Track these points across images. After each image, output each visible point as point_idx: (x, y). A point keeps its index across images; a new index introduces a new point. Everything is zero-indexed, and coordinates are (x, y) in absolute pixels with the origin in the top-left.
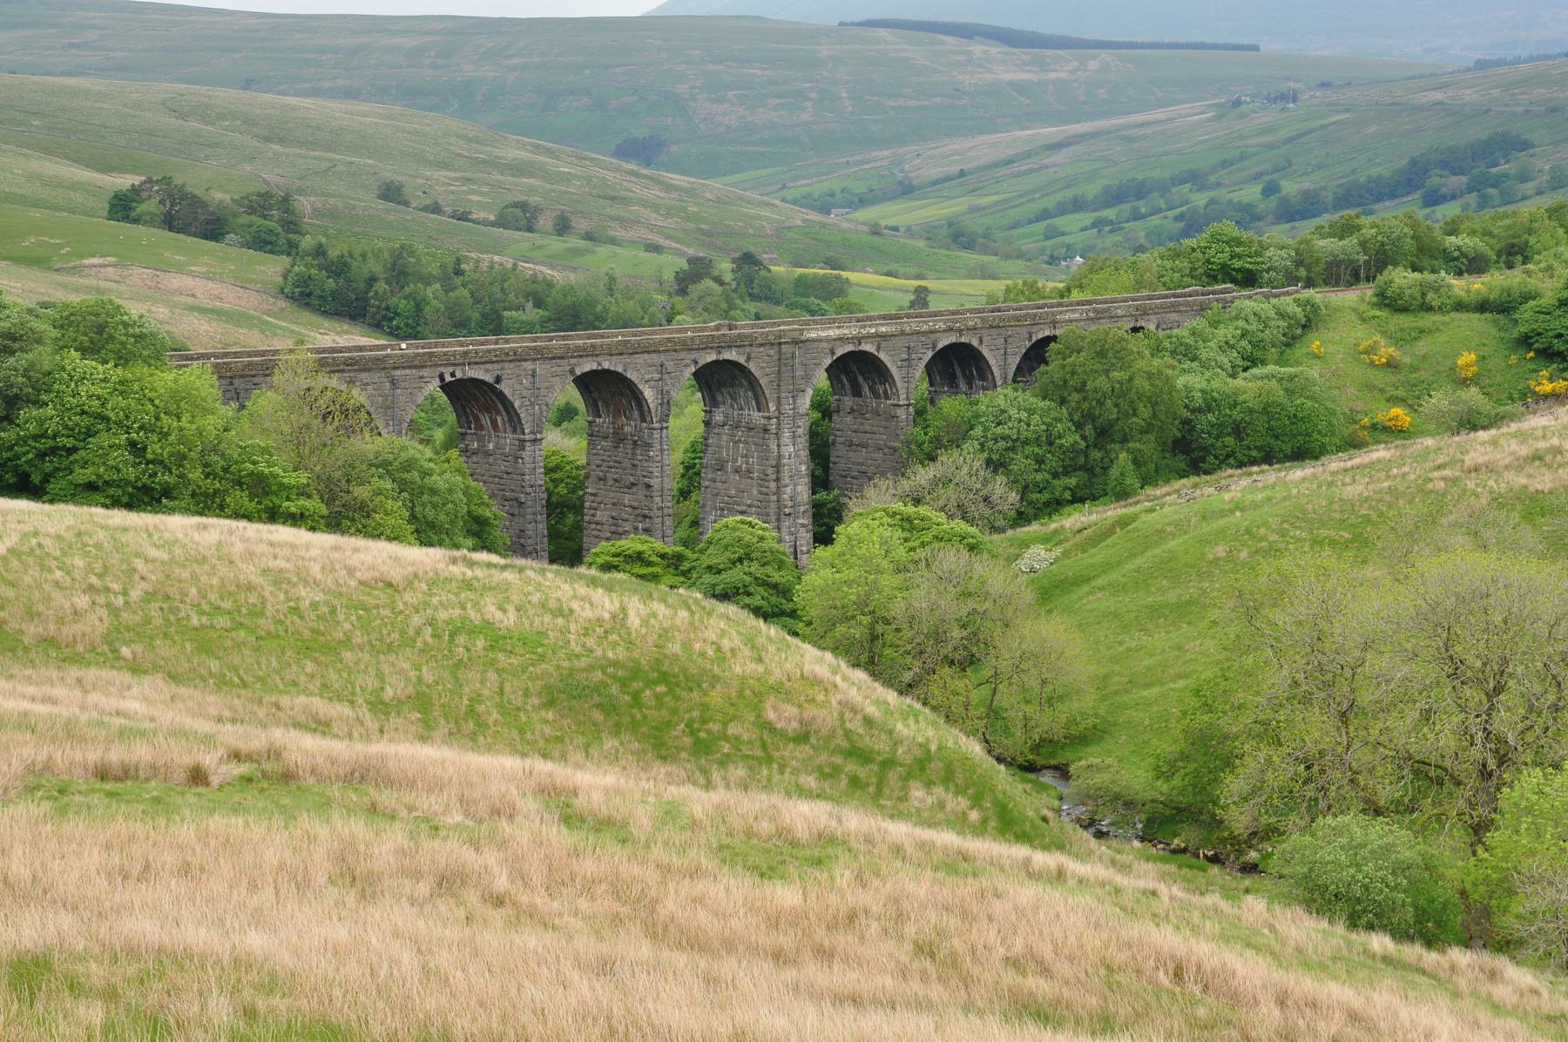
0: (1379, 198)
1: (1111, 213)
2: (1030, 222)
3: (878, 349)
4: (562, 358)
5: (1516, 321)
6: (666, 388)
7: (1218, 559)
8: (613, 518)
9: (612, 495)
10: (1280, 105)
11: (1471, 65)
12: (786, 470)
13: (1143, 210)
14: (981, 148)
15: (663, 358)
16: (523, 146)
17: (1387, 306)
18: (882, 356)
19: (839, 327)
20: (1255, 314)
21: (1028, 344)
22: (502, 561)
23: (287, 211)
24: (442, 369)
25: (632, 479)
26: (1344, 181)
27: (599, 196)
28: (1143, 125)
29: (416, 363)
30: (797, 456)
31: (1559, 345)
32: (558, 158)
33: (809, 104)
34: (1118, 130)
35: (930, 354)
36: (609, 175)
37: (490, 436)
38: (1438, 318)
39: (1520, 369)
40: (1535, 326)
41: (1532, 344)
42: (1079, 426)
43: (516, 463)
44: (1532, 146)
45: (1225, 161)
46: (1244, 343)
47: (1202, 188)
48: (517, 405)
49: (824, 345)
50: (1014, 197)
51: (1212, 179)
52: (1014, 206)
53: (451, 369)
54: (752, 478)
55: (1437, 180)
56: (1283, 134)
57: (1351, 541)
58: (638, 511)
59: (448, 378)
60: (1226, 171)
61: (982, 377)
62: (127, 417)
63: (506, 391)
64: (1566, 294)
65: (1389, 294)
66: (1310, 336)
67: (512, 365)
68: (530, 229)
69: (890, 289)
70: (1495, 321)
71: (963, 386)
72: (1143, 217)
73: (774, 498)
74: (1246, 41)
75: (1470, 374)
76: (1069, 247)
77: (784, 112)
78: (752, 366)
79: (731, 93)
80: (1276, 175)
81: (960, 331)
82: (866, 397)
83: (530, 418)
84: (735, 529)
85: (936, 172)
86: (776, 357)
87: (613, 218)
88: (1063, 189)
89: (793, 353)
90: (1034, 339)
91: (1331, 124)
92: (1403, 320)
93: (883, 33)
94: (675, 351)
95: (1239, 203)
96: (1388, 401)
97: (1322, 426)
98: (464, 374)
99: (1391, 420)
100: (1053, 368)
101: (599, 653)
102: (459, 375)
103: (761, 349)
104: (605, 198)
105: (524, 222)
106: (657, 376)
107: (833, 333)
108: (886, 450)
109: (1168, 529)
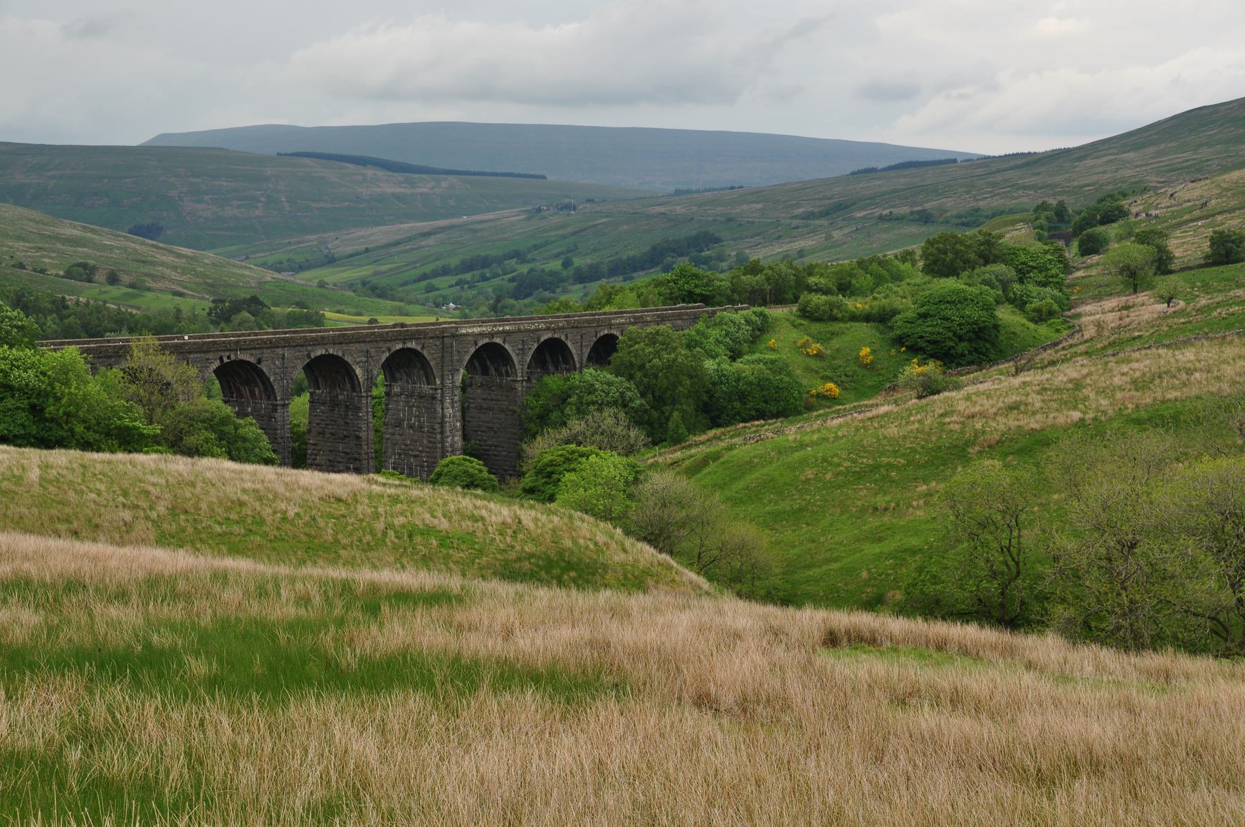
0: (635, 270)
1: (468, 276)
2: (414, 282)
3: (504, 342)
4: (302, 346)
6: (370, 368)
8: (330, 461)
9: (329, 444)
10: (566, 212)
13: (488, 275)
14: (379, 234)
17: (807, 317)
18: (507, 346)
19: (480, 326)
22: (397, 482)
24: (222, 354)
26: (612, 259)
27: (133, 260)
28: (482, 222)
34: (466, 225)
35: (536, 345)
36: (138, 247)
37: (248, 402)
38: (842, 325)
39: (898, 359)
41: (904, 343)
42: (643, 395)
43: (270, 421)
44: (722, 241)
45: (535, 246)
46: (728, 340)
47: (524, 261)
48: (272, 379)
49: (470, 338)
50: (403, 266)
51: (530, 256)
53: (227, 354)
54: (423, 432)
55: (670, 259)
56: (570, 230)
58: (351, 456)
59: (226, 360)
60: (537, 251)
63: (265, 369)
65: (808, 309)
66: (766, 336)
67: (269, 351)
68: (90, 281)
69: (346, 321)
71: (551, 368)
72: (488, 279)
73: (440, 445)
74: (538, 173)
76: (444, 297)
77: (244, 210)
78: (425, 353)
79: (206, 197)
80: (569, 255)
81: (554, 330)
82: (492, 375)
83: (281, 389)
84: (459, 465)
85: (349, 249)
86: (441, 347)
87: (146, 275)
88: (434, 261)
89: (452, 344)
90: (598, 336)
91: (600, 224)
92: (817, 327)
93: (306, 160)
94: (376, 341)
99: (827, 391)
101: (518, 548)
102: (233, 357)
103: (431, 341)
106: (364, 359)
107: (476, 330)
108: (508, 412)
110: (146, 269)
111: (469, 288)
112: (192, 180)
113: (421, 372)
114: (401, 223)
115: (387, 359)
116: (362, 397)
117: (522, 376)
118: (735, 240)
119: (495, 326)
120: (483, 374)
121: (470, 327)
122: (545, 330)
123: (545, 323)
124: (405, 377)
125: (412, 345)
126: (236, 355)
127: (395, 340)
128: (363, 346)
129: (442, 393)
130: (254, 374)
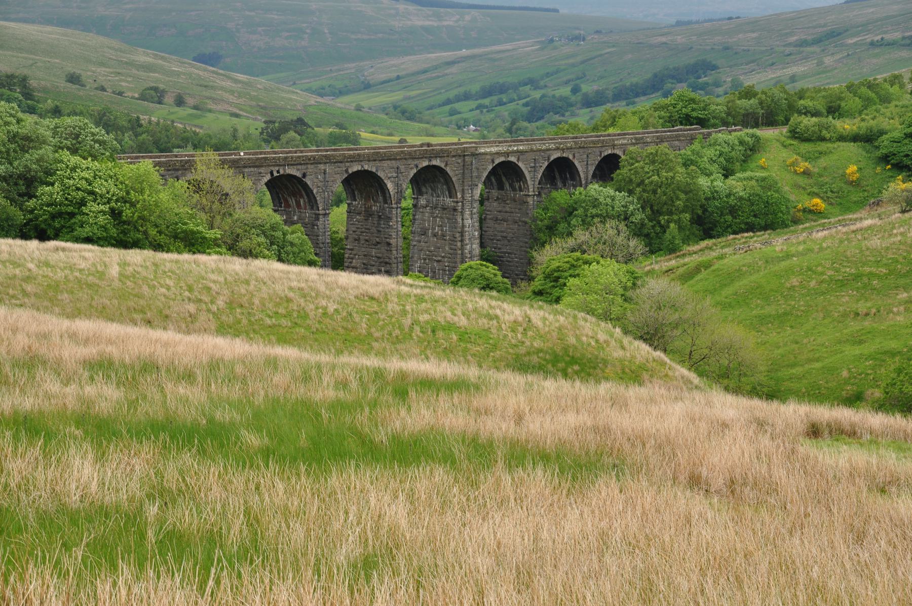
1: (486, 101)
2: (440, 106)
3: (518, 160)
5: (878, 148)
7: (794, 286)
8: (364, 264)
9: (364, 249)
11: (674, 23)
12: (467, 237)
13: (504, 100)
14: (410, 63)
15: (398, 163)
16: (148, 55)
17: (796, 138)
18: (520, 164)
19: (497, 146)
20: (726, 143)
21: (599, 158)
22: (423, 284)
23: (25, 87)
24: (272, 168)
25: (377, 239)
26: (616, 85)
29: (257, 164)
30: (473, 226)
31: (907, 161)
32: (169, 62)
33: (306, 36)
34: (486, 55)
35: (546, 164)
36: (201, 73)
38: (829, 145)
40: (892, 150)
41: (889, 161)
43: (313, 228)
44: (718, 68)
45: (548, 73)
46: (722, 159)
47: (537, 88)
48: (315, 191)
49: (488, 157)
50: (431, 92)
51: (542, 83)
52: (430, 97)
53: (277, 168)
54: (445, 240)
55: (669, 85)
56: (579, 59)
57: (889, 274)
59: (275, 174)
61: (573, 179)
62: (108, 193)
63: (309, 183)
64: (909, 130)
65: (798, 130)
66: (757, 156)
67: (312, 166)
68: (160, 103)
69: (379, 141)
70: (864, 147)
71: (560, 184)
72: (505, 104)
73: (460, 252)
75: (855, 178)
76: (465, 120)
77: (291, 41)
78: (448, 170)
79: (260, 29)
80: (578, 82)
81: (563, 150)
82: (507, 190)
83: (322, 201)
85: (383, 77)
86: (462, 164)
88: (457, 87)
89: (472, 162)
90: (603, 156)
91: (606, 53)
92: (806, 147)
94: (405, 159)
95: (561, 96)
96: (809, 194)
97: (783, 208)
98: (285, 171)
99: (813, 206)
100: (623, 172)
101: (528, 343)
102: (282, 172)
103: (454, 159)
104: (201, 86)
105: (156, 99)
106: (395, 175)
107: (494, 149)
108: (520, 223)
109: (744, 269)
110: (207, 93)
111: (488, 111)
112: (247, 13)
113: (445, 187)
114: (429, 53)
115: (415, 175)
116: (393, 208)
117: (534, 191)
118: (731, 67)
119: (510, 146)
120: (499, 189)
121: (488, 147)
122: (555, 150)
123: (555, 144)
124: (430, 191)
125: (436, 162)
126: (284, 170)
127: (422, 158)
128: (394, 163)
129: (463, 205)
130: (300, 188)
